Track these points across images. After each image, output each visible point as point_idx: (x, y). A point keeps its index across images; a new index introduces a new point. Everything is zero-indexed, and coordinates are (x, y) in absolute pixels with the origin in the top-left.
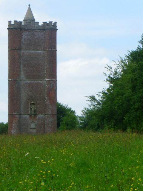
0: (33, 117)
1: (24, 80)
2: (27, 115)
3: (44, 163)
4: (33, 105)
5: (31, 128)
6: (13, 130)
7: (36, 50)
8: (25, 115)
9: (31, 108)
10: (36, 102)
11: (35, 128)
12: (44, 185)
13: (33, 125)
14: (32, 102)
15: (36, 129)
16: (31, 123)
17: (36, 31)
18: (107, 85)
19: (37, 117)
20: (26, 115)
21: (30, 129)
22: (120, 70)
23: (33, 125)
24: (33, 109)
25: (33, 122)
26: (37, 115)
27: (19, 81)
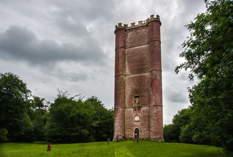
6: (116, 123)
7: (140, 46)
8: (130, 108)
11: (139, 121)
13: (137, 118)
14: (137, 95)
17: (140, 29)
20: (130, 109)
21: (134, 122)
24: (137, 102)
25: (137, 115)
26: (141, 107)
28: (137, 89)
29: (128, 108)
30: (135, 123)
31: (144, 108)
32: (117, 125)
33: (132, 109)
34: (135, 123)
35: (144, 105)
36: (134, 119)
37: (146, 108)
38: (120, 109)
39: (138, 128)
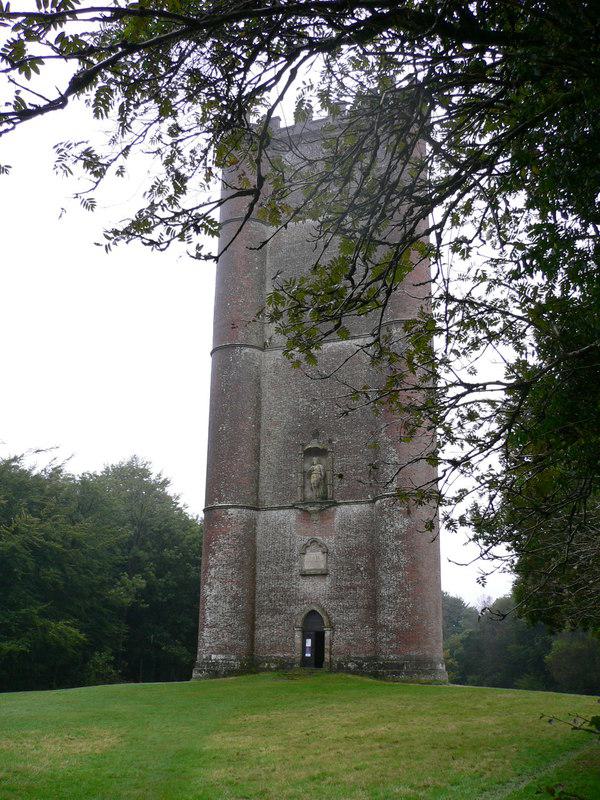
0: (315, 517)
1: (470, 678)
2: (287, 511)
3: (542, 356)
4: (315, 459)
5: (304, 575)
6: (209, 584)
8: (279, 508)
9: (308, 474)
10: (330, 441)
11: (324, 575)
12: (524, 191)
14: (313, 444)
15: (328, 581)
16: (306, 546)
18: (513, 577)
19: (337, 519)
22: (470, 606)
23: (314, 560)
25: (314, 541)
26: (336, 504)
27: (247, 350)
28: (317, 414)
29: (272, 509)
30: (307, 587)
31: (347, 506)
32: (214, 593)
33: (292, 516)
34: (307, 587)
35: (353, 496)
36: (302, 563)
37: (356, 508)
38: (230, 511)
39: (315, 608)
